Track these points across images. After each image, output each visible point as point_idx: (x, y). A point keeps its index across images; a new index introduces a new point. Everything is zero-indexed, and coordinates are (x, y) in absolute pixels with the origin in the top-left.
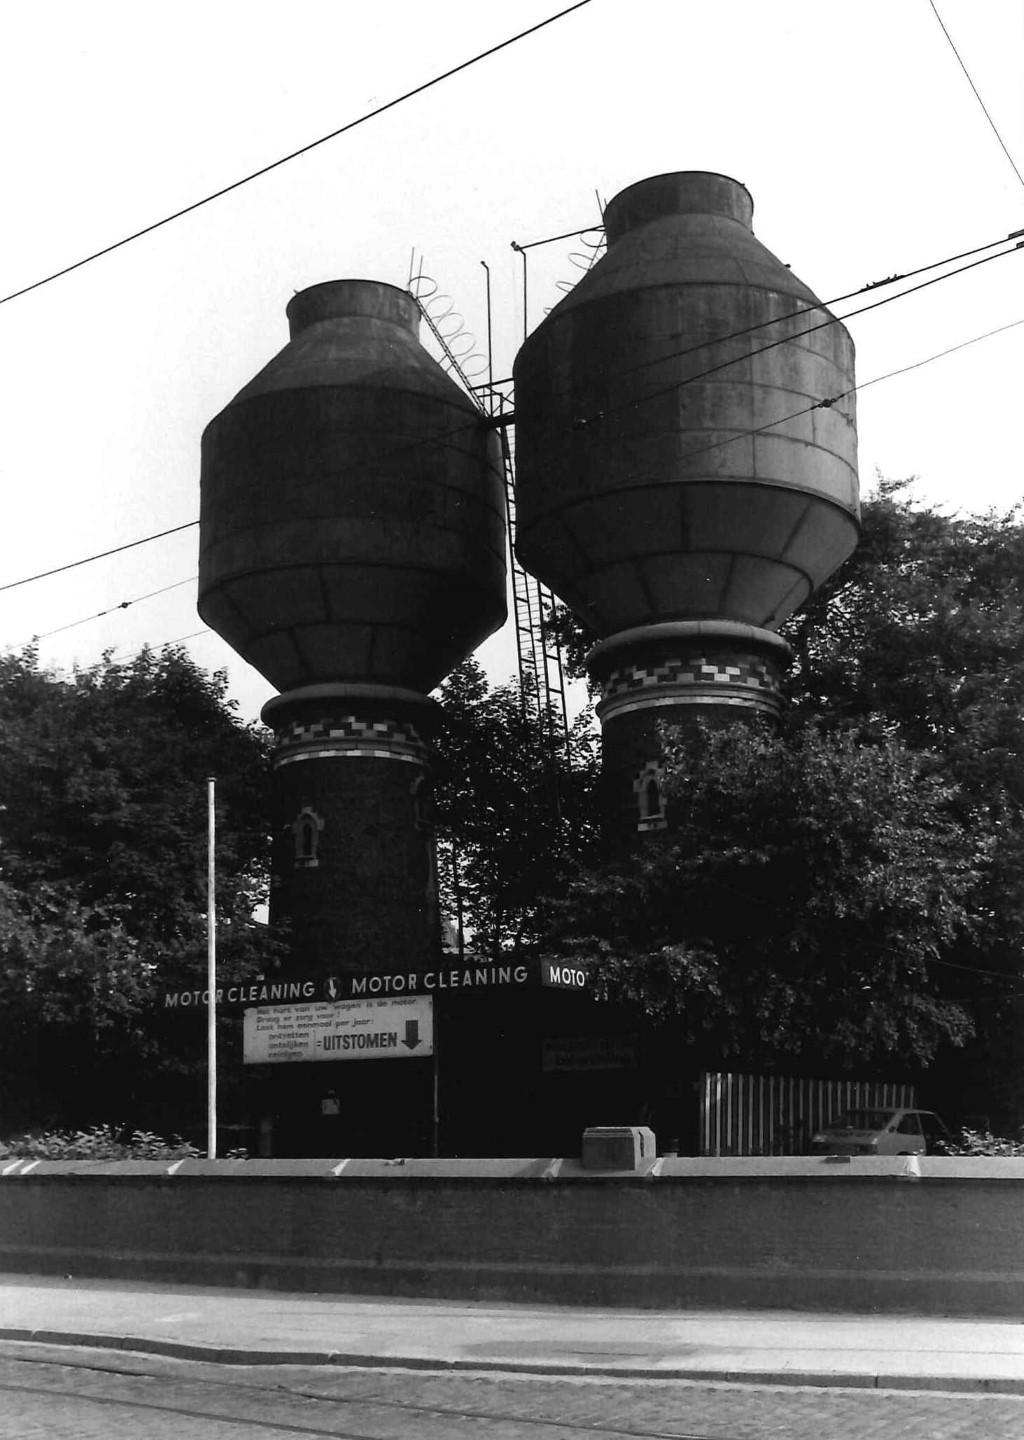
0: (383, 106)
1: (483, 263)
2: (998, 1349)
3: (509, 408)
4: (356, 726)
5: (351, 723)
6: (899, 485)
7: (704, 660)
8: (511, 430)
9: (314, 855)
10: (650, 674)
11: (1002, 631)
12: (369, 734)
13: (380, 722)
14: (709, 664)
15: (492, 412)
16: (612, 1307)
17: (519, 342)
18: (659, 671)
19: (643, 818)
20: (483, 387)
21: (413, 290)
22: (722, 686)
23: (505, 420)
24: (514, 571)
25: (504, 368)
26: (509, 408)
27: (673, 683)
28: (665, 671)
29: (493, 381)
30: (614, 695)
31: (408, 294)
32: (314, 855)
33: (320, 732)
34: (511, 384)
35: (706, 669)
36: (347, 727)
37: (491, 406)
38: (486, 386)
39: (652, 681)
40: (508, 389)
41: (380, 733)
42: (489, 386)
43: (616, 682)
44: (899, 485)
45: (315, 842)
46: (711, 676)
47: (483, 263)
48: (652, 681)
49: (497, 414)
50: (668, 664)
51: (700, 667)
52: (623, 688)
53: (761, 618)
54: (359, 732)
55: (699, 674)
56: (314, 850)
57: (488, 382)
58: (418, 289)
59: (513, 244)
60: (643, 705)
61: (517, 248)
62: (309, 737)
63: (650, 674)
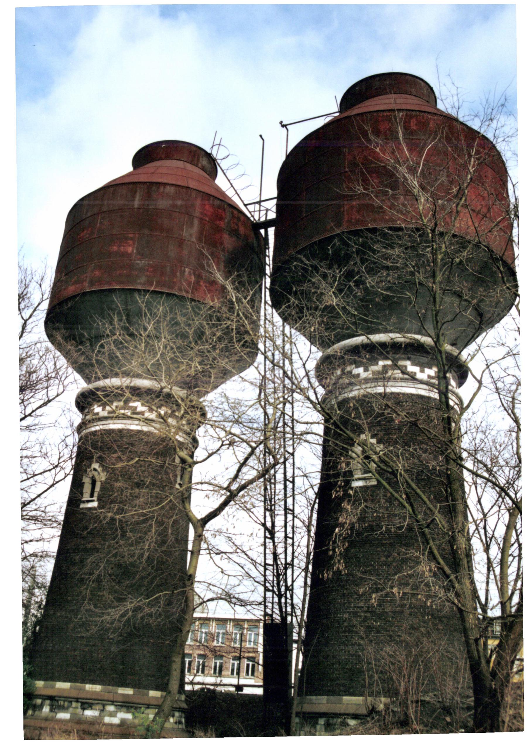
1: (261, 136)
2: (267, 555)
3: (272, 215)
6: (519, 311)
8: (271, 231)
9: (95, 498)
15: (260, 218)
16: (351, 346)
17: (282, 158)
19: (356, 476)
20: (254, 203)
21: (214, 154)
22: (421, 382)
23: (267, 224)
24: (266, 302)
25: (271, 190)
26: (272, 215)
29: (262, 199)
31: (209, 156)
32: (95, 498)
34: (275, 201)
37: (257, 215)
40: (272, 205)
42: (259, 203)
44: (519, 311)
45: (97, 489)
47: (261, 136)
49: (263, 219)
54: (142, 413)
56: (96, 494)
57: (258, 200)
58: (218, 154)
61: (283, 126)
62: (105, 414)
63: (366, 370)
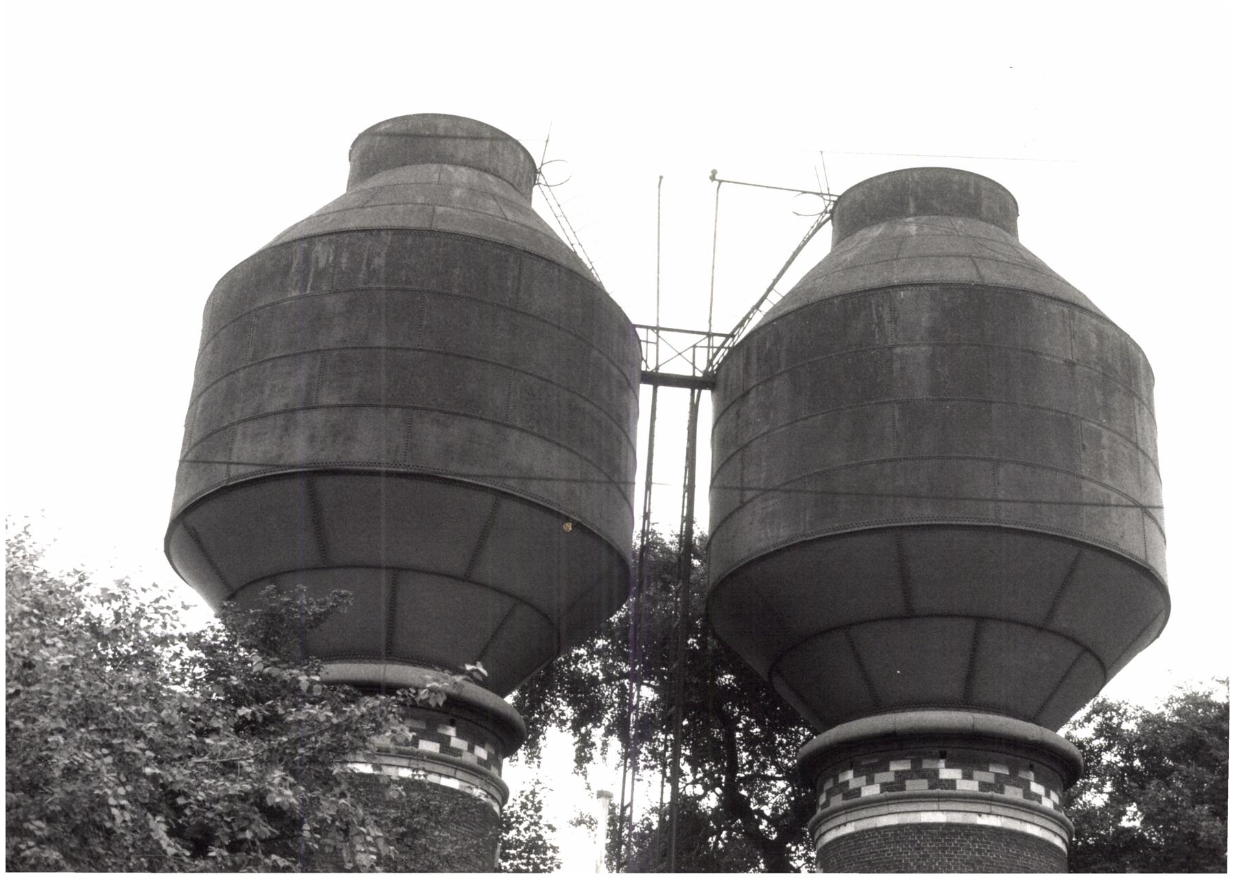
0: (799, 241)
1: (661, 178)
4: (456, 743)
5: (449, 737)
7: (942, 764)
10: (968, 776)
11: (569, 724)
12: (467, 758)
13: (482, 745)
14: (1038, 781)
18: (978, 775)
27: (901, 793)
28: (989, 777)
30: (483, 768)
33: (990, 784)
35: (946, 774)
36: (444, 741)
38: (653, 328)
39: (971, 786)
41: (480, 760)
43: (902, 777)
46: (951, 783)
47: (661, 178)
48: (969, 787)
50: (992, 769)
51: (936, 772)
52: (917, 786)
53: (954, 688)
54: (458, 752)
55: (935, 782)
59: (714, 172)
60: (957, 818)
